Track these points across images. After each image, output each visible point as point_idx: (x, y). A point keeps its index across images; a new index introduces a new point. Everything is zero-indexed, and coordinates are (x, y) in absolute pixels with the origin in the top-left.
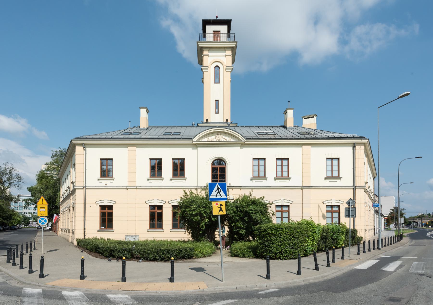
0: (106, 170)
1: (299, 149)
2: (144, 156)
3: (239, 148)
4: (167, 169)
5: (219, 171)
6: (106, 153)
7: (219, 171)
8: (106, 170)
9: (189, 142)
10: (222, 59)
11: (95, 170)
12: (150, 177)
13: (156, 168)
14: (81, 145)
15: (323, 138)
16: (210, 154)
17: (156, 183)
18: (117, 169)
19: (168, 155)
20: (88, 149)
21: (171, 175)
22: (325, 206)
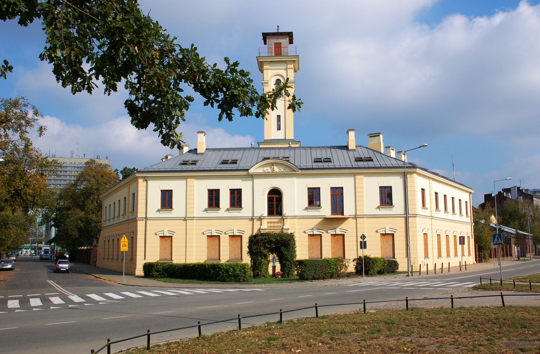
0: (167, 199)
1: (183, 182)
2: (200, 188)
3: (240, 180)
4: (225, 200)
5: (275, 200)
6: (167, 185)
7: (275, 200)
8: (167, 199)
9: (244, 173)
10: (283, 73)
11: (156, 201)
12: (208, 208)
13: (214, 198)
14: (141, 177)
15: (433, 173)
16: (263, 187)
17: (213, 214)
18: (177, 200)
19: (225, 187)
20: (149, 182)
21: (228, 206)
22: (379, 235)
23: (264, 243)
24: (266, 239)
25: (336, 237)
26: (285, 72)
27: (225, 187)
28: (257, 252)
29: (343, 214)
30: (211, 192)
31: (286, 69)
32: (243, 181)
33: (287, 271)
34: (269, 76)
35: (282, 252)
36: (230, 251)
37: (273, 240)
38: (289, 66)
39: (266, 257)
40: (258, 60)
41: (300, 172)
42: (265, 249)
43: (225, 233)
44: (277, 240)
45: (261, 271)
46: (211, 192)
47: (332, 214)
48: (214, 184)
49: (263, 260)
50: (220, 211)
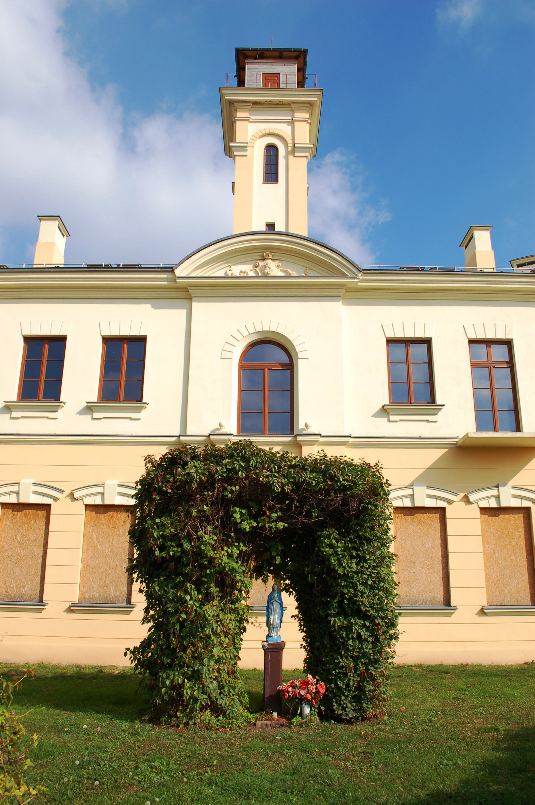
3: (149, 306)
9: (160, 280)
10: (285, 130)
23: (225, 504)
24: (230, 478)
25: (504, 517)
26: (290, 128)
27: (84, 329)
28: (177, 560)
29: (518, 429)
30: (33, 343)
31: (292, 123)
32: (155, 307)
33: (353, 680)
34: (250, 136)
35: (324, 560)
36: (86, 568)
37: (278, 483)
38: (297, 115)
39: (227, 586)
40: (221, 96)
41: (360, 281)
42: (225, 542)
43: (72, 496)
44: (297, 485)
45: (196, 676)
46: (33, 343)
47: (480, 427)
48: (46, 318)
49: (210, 610)
50: (59, 414)
